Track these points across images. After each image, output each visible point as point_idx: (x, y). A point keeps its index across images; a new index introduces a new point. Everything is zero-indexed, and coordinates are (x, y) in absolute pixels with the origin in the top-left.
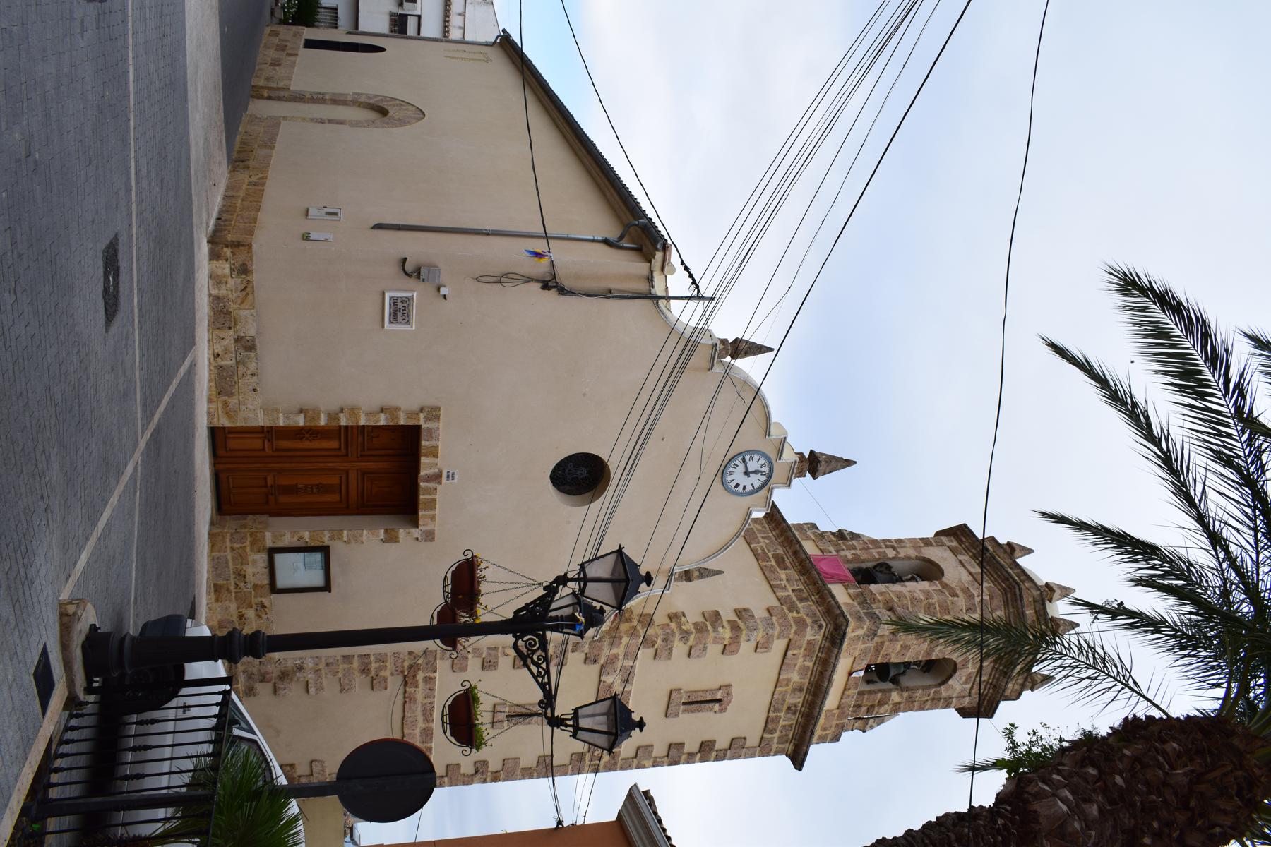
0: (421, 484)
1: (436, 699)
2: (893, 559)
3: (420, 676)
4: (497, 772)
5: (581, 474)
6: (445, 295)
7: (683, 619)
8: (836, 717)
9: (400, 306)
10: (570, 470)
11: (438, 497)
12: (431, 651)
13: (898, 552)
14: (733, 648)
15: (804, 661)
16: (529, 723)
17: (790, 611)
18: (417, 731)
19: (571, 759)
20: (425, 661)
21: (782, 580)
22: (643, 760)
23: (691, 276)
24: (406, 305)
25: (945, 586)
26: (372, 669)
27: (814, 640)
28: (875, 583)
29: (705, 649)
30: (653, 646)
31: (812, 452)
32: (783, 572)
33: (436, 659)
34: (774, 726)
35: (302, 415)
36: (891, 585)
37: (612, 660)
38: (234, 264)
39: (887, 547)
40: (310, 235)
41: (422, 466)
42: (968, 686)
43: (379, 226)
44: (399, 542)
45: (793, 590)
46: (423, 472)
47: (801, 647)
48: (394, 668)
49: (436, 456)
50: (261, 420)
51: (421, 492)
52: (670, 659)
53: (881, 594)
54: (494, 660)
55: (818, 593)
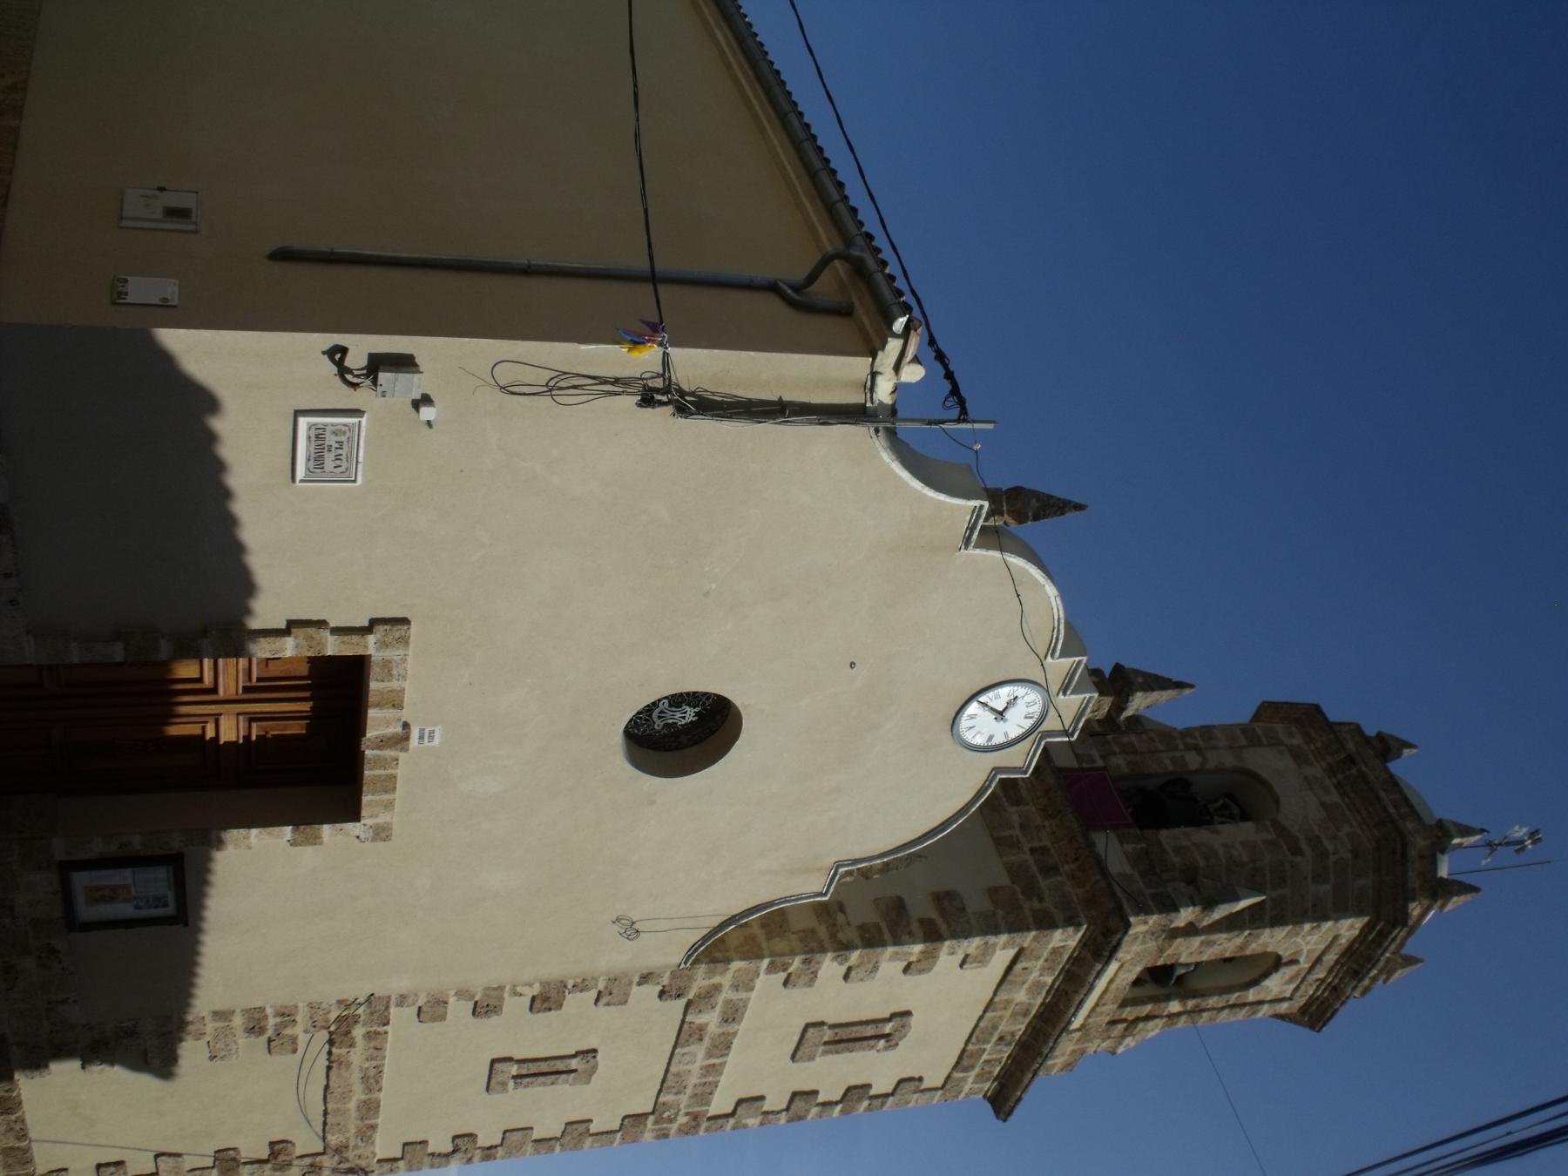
0: (368, 752)
1: (386, 1061)
2: (1197, 772)
3: (358, 1032)
4: (491, 1148)
5: (684, 718)
6: (428, 421)
7: (840, 918)
9: (331, 440)
10: (662, 712)
11: (401, 771)
12: (379, 998)
13: (1205, 759)
15: (1041, 975)
16: (553, 1084)
18: (352, 1105)
20: (368, 1011)
21: (1012, 827)
24: (343, 438)
25: (1281, 830)
26: (268, 1027)
28: (1166, 824)
30: (784, 970)
31: (1118, 668)
32: (1014, 809)
33: (387, 1008)
37: (709, 994)
39: (1188, 748)
41: (369, 722)
42: (1292, 986)
43: (284, 255)
44: (321, 843)
45: (1032, 850)
47: (1039, 958)
48: (310, 1023)
51: (366, 766)
53: (1178, 850)
54: (497, 1003)
55: (1076, 860)
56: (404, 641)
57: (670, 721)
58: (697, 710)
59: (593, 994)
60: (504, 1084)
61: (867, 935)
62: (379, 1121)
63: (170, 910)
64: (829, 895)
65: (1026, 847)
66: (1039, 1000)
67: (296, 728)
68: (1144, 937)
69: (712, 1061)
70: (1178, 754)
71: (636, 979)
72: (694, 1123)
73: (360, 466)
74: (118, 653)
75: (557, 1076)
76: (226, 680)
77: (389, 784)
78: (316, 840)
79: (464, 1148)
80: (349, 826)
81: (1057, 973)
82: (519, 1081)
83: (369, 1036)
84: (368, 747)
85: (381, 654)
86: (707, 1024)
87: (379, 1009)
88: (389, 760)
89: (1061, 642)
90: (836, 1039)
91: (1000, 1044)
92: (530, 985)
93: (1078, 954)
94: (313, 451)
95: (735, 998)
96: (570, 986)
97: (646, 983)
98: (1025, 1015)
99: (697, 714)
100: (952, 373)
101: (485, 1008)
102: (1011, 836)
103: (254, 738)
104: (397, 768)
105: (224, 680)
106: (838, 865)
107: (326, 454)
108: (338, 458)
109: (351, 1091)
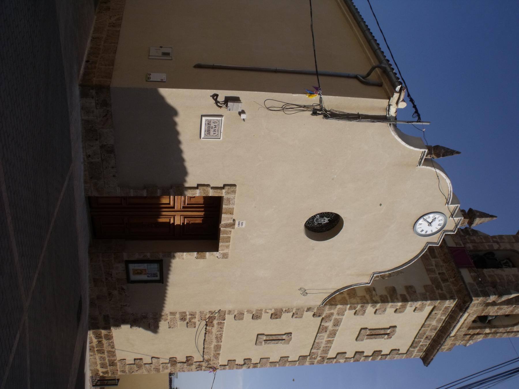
1: (224, 332)
2: (497, 250)
3: (215, 322)
5: (324, 221)
6: (244, 119)
7: (374, 293)
8: (452, 340)
9: (212, 125)
10: (317, 219)
11: (232, 236)
12: (222, 311)
13: (500, 245)
14: (401, 310)
15: (441, 316)
16: (277, 343)
17: (438, 289)
18: (212, 346)
19: (299, 359)
20: (218, 316)
21: (432, 266)
22: (340, 359)
23: (415, 106)
27: (449, 306)
29: (385, 310)
30: (355, 309)
32: (433, 259)
33: (225, 315)
34: (416, 345)
35: (145, 191)
36: (496, 269)
38: (98, 100)
39: (494, 242)
40: (151, 76)
43: (198, 66)
44: (206, 258)
45: (439, 274)
46: (223, 222)
48: (200, 318)
49: (232, 213)
50: (119, 192)
52: (363, 315)
53: (490, 276)
55: (454, 277)
56: (234, 192)
57: (320, 222)
58: (329, 219)
59: (291, 314)
60: (261, 343)
61: (383, 299)
62: (221, 352)
63: (158, 278)
64: (370, 284)
65: (437, 272)
66: (440, 325)
67: (199, 221)
68: (477, 305)
69: (329, 339)
70: (490, 244)
71: (306, 310)
72: (322, 360)
73: (221, 133)
74: (145, 193)
75: (279, 341)
76: (177, 204)
77: (228, 240)
78: (204, 257)
79: (247, 363)
80: (215, 253)
81: (447, 316)
82: (266, 342)
83: (219, 324)
84: (222, 227)
85: (226, 196)
86: (328, 326)
87: (222, 315)
88: (228, 231)
89: (451, 199)
90: (371, 334)
91: (426, 339)
92: (271, 310)
93: (454, 309)
94: (207, 128)
95: (338, 318)
96: (284, 311)
97: (309, 311)
98: (435, 330)
99: (329, 220)
100: (416, 105)
101: (256, 317)
102: (432, 268)
103: (185, 224)
104: (231, 234)
105: (177, 204)
106: (374, 273)
107: (211, 130)
108: (215, 131)
109: (212, 342)
